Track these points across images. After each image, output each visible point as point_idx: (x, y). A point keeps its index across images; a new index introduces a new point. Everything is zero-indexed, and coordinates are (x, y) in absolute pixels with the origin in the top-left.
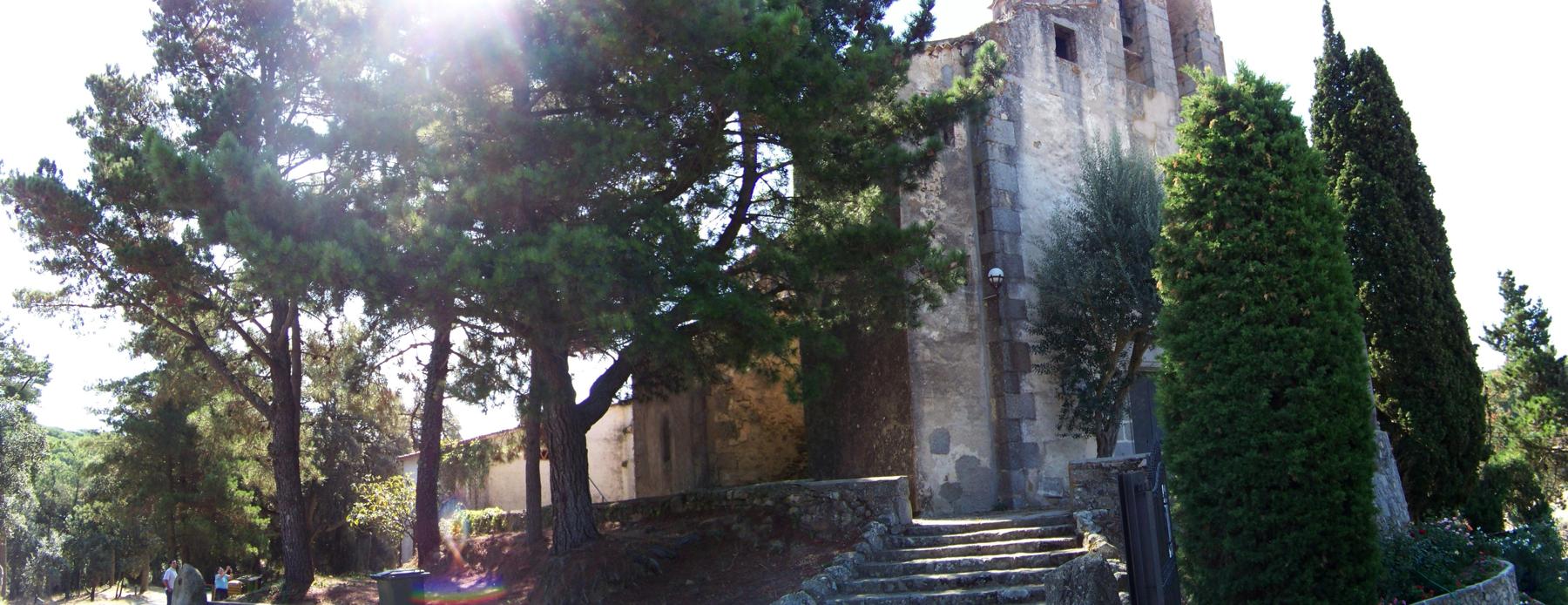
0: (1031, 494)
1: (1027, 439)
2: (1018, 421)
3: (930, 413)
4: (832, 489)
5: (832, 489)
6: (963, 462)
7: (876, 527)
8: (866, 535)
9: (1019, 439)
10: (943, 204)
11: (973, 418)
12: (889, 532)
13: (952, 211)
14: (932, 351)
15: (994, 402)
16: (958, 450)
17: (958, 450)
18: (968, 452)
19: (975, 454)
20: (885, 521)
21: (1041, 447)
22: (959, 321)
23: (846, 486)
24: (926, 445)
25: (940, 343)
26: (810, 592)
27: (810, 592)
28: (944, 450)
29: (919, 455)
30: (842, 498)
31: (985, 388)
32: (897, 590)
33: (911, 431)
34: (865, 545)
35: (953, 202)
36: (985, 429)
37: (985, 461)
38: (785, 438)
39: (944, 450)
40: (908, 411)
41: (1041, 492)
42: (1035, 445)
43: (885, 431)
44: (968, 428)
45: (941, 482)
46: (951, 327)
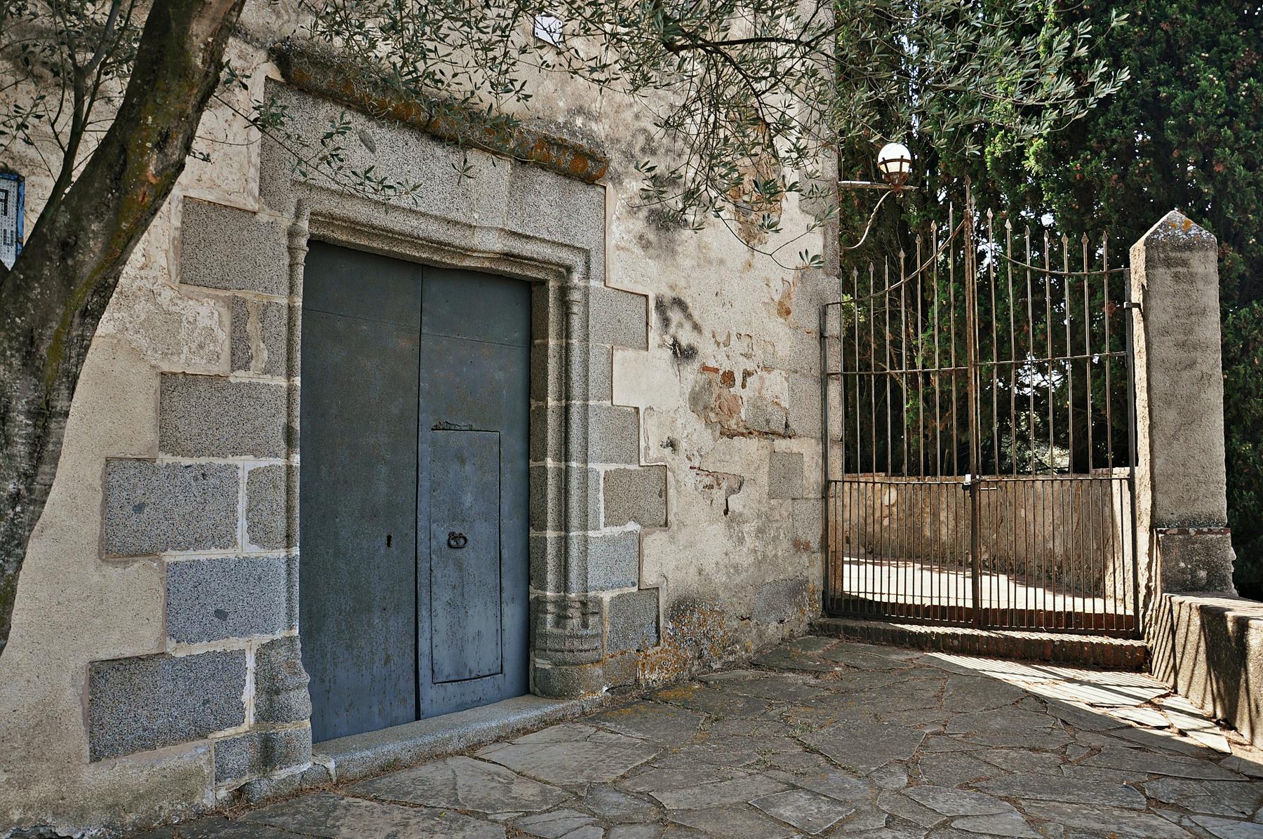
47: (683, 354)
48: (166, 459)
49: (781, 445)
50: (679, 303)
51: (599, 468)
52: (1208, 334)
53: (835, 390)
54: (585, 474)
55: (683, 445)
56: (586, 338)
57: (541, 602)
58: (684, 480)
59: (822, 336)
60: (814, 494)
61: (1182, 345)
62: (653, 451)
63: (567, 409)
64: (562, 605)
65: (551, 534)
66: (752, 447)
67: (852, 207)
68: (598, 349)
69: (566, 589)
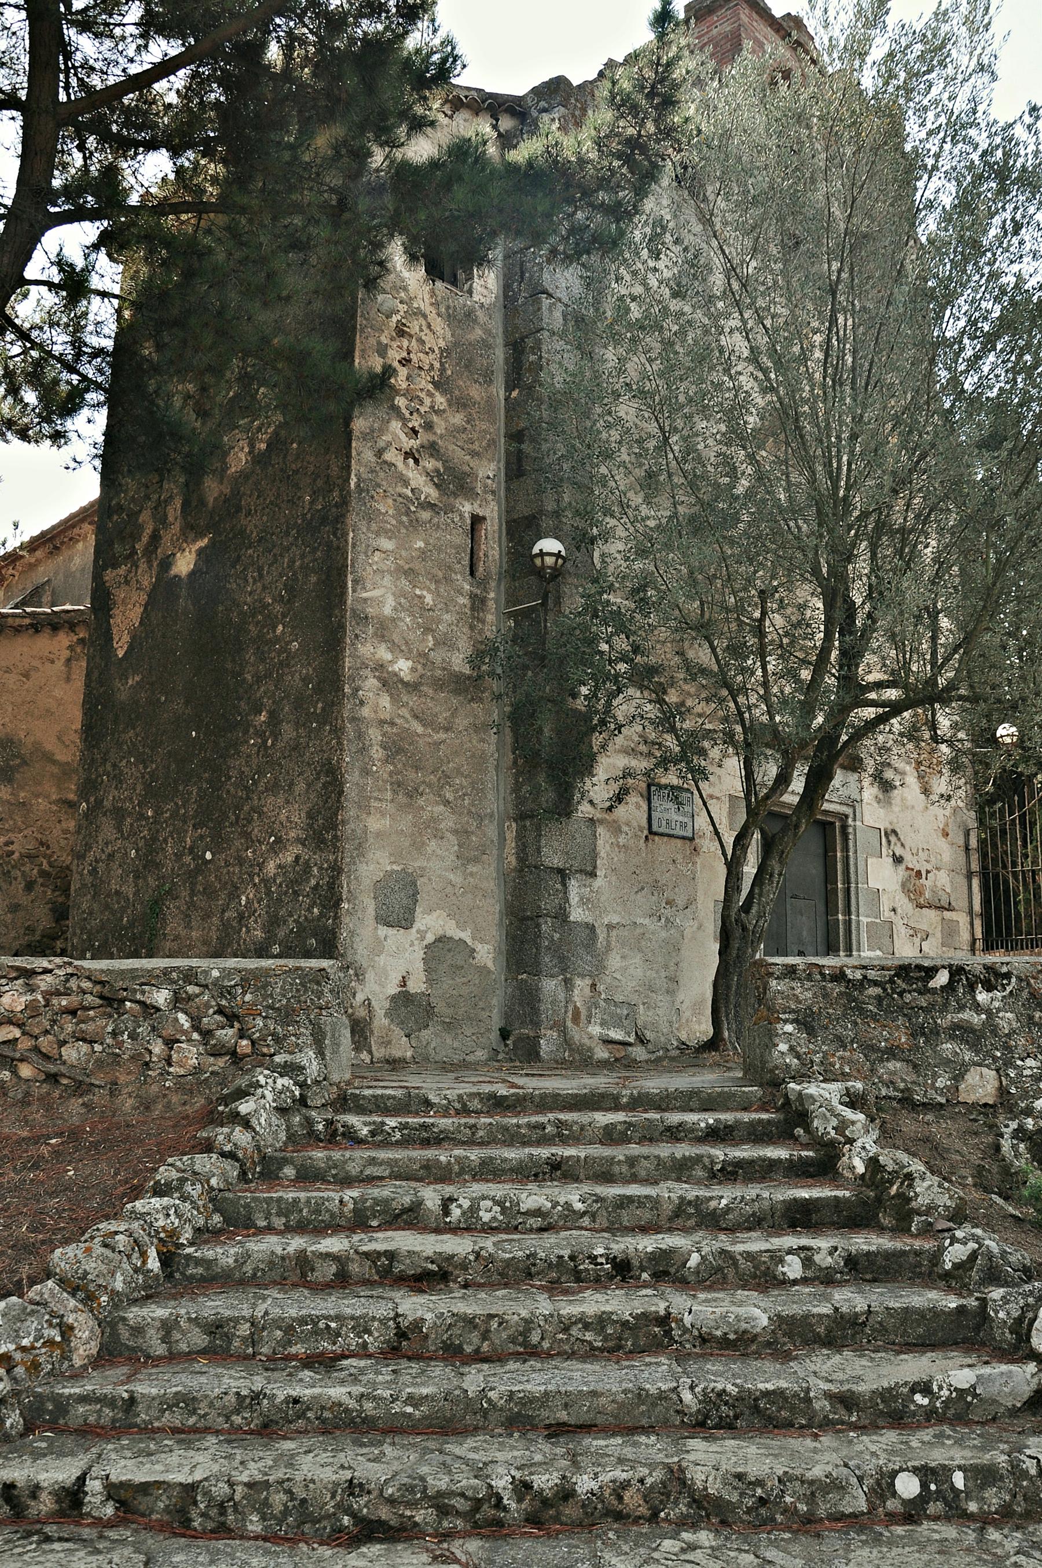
0: (575, 1033)
1: (577, 914)
2: (563, 874)
3: (378, 834)
4: (154, 979)
5: (154, 979)
6: (440, 952)
7: (272, 1086)
8: (245, 1107)
9: (561, 915)
10: (440, 400)
11: (466, 858)
12: (303, 1101)
13: (458, 419)
14: (395, 699)
15: (511, 830)
16: (432, 922)
17: (432, 922)
18: (453, 931)
19: (466, 935)
20: (291, 1069)
21: (601, 934)
22: (452, 647)
23: (190, 976)
24: (369, 906)
25: (413, 687)
26: (77, 1286)
27: (77, 1286)
28: (404, 921)
29: (348, 922)
30: (178, 1001)
31: (496, 799)
32: (342, 1281)
33: (336, 870)
34: (241, 1137)
35: (460, 403)
36: (491, 885)
37: (486, 954)
38: (29, 886)
39: (404, 921)
40: (332, 824)
41: (595, 1030)
42: (592, 928)
43: (271, 867)
44: (456, 878)
45: (393, 989)
46: (437, 657)
47: (898, 860)
49: (947, 915)
50: (894, 832)
51: (864, 920)
54: (858, 922)
55: (899, 911)
56: (856, 852)
59: (967, 849)
62: (887, 914)
63: (849, 888)
66: (932, 914)
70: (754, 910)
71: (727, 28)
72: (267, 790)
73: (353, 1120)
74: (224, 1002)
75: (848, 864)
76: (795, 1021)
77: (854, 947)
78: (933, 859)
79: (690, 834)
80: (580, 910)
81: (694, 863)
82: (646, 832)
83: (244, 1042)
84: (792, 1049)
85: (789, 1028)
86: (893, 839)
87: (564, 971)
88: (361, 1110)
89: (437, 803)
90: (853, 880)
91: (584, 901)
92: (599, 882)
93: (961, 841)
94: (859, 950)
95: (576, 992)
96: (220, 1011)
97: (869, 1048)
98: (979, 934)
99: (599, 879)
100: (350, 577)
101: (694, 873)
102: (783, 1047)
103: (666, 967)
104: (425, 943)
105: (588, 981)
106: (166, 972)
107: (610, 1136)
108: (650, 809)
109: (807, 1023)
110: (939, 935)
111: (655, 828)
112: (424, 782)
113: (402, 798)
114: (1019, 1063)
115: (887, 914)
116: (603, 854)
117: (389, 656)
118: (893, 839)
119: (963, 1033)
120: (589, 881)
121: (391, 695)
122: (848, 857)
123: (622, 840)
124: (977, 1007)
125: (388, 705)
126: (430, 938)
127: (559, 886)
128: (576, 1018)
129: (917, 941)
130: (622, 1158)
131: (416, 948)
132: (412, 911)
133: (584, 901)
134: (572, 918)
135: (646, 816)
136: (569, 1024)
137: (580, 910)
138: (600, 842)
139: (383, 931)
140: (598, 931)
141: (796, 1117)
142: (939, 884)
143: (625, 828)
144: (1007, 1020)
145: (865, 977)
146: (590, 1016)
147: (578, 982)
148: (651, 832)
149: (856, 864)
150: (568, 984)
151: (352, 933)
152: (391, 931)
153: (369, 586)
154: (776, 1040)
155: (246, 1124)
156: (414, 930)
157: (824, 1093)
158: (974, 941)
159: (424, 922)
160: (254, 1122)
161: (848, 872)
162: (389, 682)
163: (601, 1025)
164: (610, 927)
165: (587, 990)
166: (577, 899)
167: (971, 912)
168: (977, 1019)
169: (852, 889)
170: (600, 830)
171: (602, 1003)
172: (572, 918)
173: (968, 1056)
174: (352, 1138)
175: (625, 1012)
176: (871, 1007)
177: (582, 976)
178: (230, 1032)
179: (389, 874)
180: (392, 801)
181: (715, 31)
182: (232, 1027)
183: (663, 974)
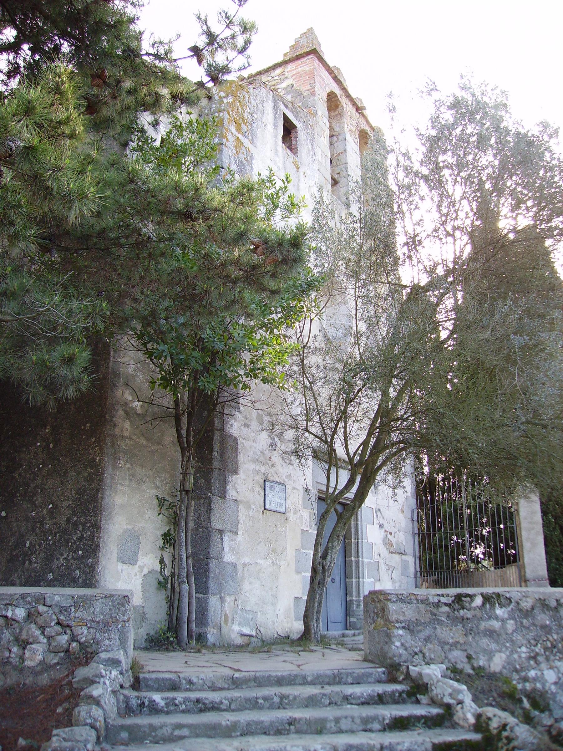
21: (240, 568)
34: (97, 712)
47: (381, 526)
48: (302, 550)
49: (404, 557)
50: (379, 510)
51: (366, 560)
52: (64, 642)
53: (417, 537)
54: (363, 562)
55: (382, 555)
56: (362, 521)
57: (351, 601)
58: (383, 567)
59: (412, 520)
60: (413, 576)
61: (531, 523)
62: (376, 557)
63: (358, 542)
64: (358, 601)
65: (354, 580)
66: (397, 557)
67: (418, 483)
68: (364, 524)
69: (359, 597)
70: (329, 557)
71: (307, 68)
72: (48, 475)
73: (157, 697)
74: (62, 617)
75: (357, 529)
76: (404, 628)
77: (361, 576)
78: (397, 525)
79: (283, 510)
80: (229, 555)
81: (286, 528)
82: (263, 509)
83: (74, 644)
84: (402, 644)
85: (401, 632)
86: (379, 514)
87: (220, 592)
88: (158, 690)
89: (152, 488)
90: (360, 537)
91: (232, 549)
92: (239, 538)
93: (410, 517)
94: (363, 578)
95: (227, 605)
96: (59, 623)
97: (443, 643)
98: (418, 569)
99: (239, 536)
100: (112, 350)
101: (285, 533)
102: (398, 644)
103: (271, 589)
104: (143, 574)
105: (233, 598)
106: (23, 596)
107: (311, 702)
108: (265, 495)
109: (409, 628)
110: (400, 569)
111: (267, 507)
112: (146, 475)
113: (134, 484)
114: (519, 650)
115: (376, 557)
116: (241, 521)
117: (130, 398)
118: (379, 514)
119: (491, 633)
120: (234, 537)
121: (131, 421)
122: (357, 524)
123: (251, 514)
124: (497, 618)
125: (129, 428)
126: (146, 571)
127: (219, 540)
128: (226, 621)
129: (390, 572)
130: (331, 718)
131: (138, 577)
132: (136, 554)
133: (232, 549)
134: (225, 560)
135: (263, 499)
136: (222, 623)
137: (229, 555)
138: (240, 514)
139: (120, 566)
140: (238, 568)
141: (418, 689)
142: (400, 541)
143: (253, 506)
144: (511, 625)
145: (439, 601)
146: (233, 620)
147: (227, 598)
148: (265, 509)
149: (362, 528)
150: (222, 600)
151: (104, 567)
152: (125, 566)
153: (122, 355)
154: (394, 639)
155: (98, 703)
156: (137, 566)
157: (433, 672)
158: (416, 572)
159: (143, 561)
160: (102, 703)
161: (358, 533)
162: (129, 414)
163: (239, 624)
164: (244, 565)
165: (232, 603)
166: (228, 548)
167: (415, 556)
168: (496, 625)
169: (360, 543)
170: (240, 507)
171: (239, 612)
172: (225, 560)
173: (493, 646)
174: (154, 709)
175: (251, 617)
176: (443, 619)
177: (230, 595)
178: (66, 637)
179: (125, 531)
180: (129, 486)
181: (300, 69)
182: (66, 633)
183: (270, 593)
